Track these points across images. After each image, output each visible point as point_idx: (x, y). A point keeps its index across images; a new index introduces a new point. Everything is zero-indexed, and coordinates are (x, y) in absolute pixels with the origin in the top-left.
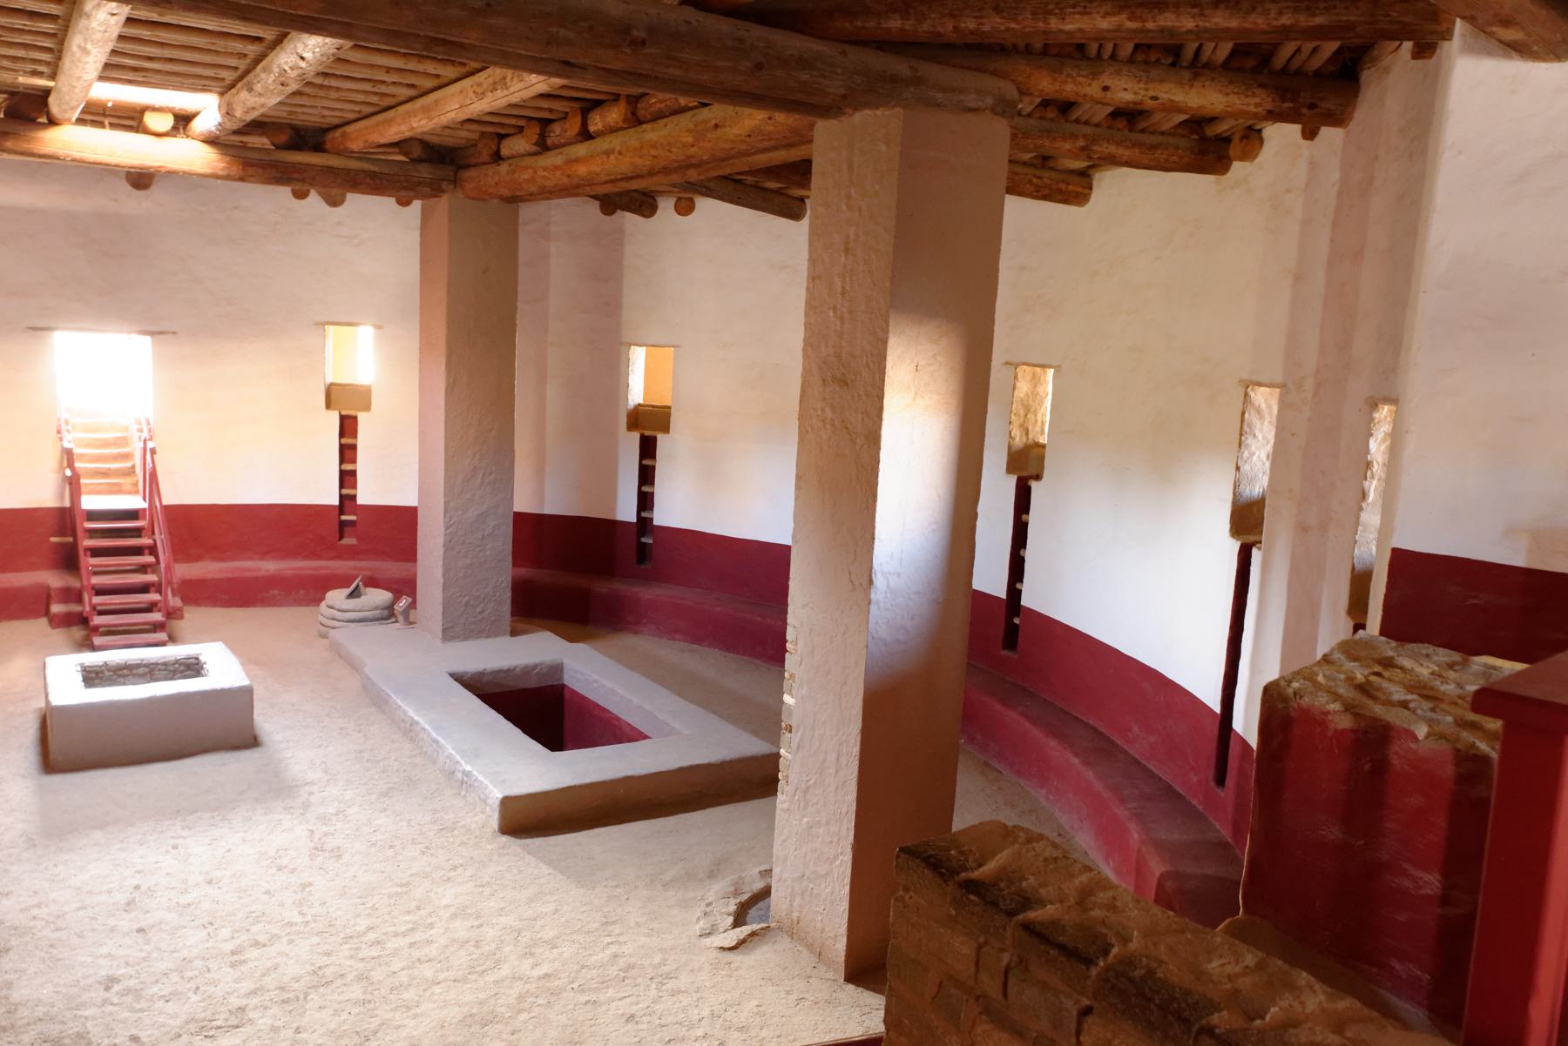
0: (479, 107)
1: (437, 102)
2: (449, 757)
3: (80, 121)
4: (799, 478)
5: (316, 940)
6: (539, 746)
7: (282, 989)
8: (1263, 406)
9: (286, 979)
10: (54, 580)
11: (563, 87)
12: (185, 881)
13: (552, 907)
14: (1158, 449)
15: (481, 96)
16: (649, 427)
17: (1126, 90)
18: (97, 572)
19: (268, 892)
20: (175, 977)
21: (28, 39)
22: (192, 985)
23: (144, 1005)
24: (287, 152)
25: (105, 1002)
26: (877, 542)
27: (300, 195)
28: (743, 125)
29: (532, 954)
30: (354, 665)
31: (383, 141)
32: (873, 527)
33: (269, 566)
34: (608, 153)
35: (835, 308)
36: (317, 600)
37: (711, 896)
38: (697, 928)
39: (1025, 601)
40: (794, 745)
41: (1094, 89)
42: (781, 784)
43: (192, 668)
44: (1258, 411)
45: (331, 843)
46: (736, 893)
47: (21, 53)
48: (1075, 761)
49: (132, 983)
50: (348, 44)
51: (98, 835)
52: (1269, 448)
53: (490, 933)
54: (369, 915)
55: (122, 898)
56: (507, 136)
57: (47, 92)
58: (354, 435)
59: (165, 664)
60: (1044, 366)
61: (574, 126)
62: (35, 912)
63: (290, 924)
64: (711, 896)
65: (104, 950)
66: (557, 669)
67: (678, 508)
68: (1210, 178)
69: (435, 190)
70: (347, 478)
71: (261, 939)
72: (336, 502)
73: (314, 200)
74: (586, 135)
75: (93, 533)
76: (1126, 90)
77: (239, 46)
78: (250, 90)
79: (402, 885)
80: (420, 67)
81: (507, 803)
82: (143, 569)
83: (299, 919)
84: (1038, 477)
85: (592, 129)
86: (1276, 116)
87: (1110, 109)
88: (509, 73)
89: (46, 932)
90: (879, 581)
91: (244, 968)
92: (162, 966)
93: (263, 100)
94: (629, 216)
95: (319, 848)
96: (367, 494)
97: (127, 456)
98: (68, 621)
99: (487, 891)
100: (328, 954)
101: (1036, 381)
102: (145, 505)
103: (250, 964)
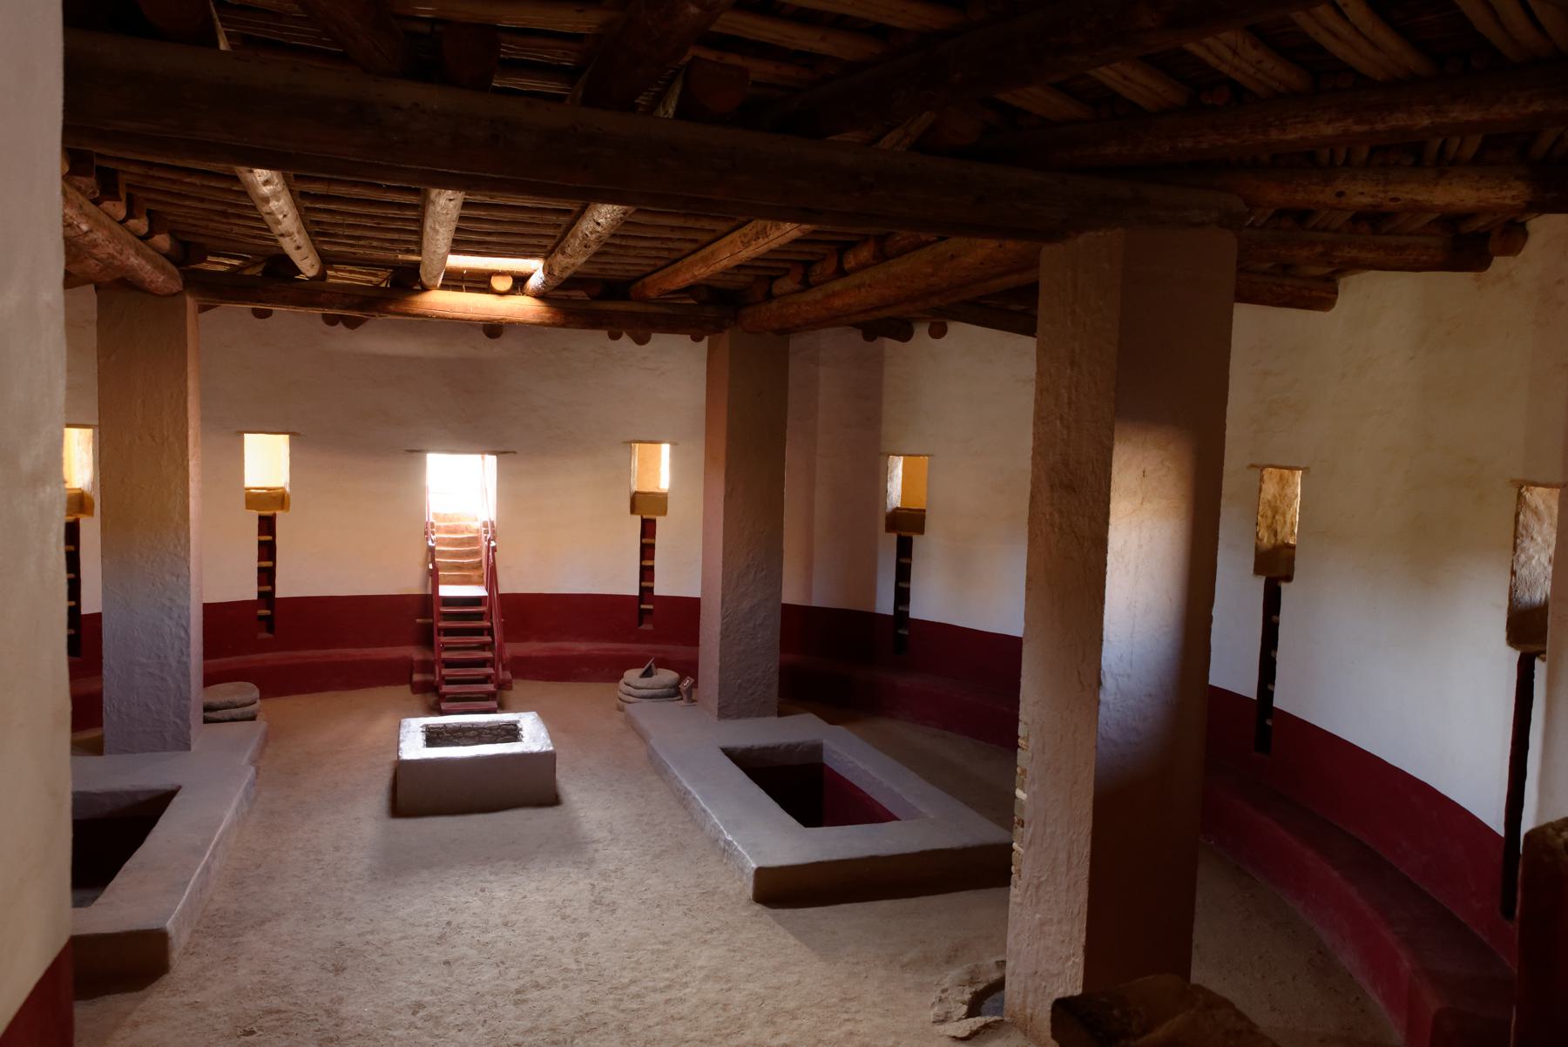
0: (746, 254)
1: (713, 253)
2: (714, 826)
3: (444, 287)
4: (1029, 579)
5: (586, 987)
6: (794, 821)
7: (553, 1030)
8: (1542, 507)
9: (558, 1021)
10: (416, 654)
11: (814, 232)
12: (487, 922)
13: (795, 978)
14: (1426, 547)
15: (746, 245)
16: (907, 525)
17: (1362, 193)
18: (449, 648)
19: (551, 938)
20: (468, 1009)
21: (399, 225)
22: (481, 1017)
23: (440, 1032)
24: (593, 302)
25: (412, 1025)
26: (1105, 643)
27: (615, 336)
28: (977, 252)
29: (774, 1023)
30: (643, 737)
31: (673, 288)
32: (1101, 630)
33: (582, 647)
34: (859, 287)
35: (1061, 418)
36: (617, 678)
37: (946, 983)
38: (931, 1014)
39: (1278, 702)
40: (1027, 837)
41: (1327, 196)
42: (1014, 877)
43: (511, 733)
44: (1536, 512)
45: (609, 897)
46: (972, 982)
47: (396, 236)
48: (1335, 874)
49: (434, 1010)
50: (631, 209)
51: (425, 874)
52: (1551, 551)
53: (737, 997)
54: (633, 969)
55: (435, 931)
56: (777, 277)
57: (417, 265)
58: (653, 535)
59: (491, 729)
60: (1292, 469)
61: (830, 266)
62: (369, 937)
63: (567, 970)
64: (946, 983)
65: (416, 978)
66: (817, 749)
67: (935, 600)
68: (1471, 275)
69: (718, 328)
70: (647, 573)
71: (542, 981)
72: (636, 593)
73: (625, 341)
74: (841, 272)
75: (448, 616)
76: (1362, 193)
77: (553, 218)
78: (563, 253)
79: (664, 943)
80: (698, 225)
81: (761, 873)
82: (483, 647)
83: (574, 966)
84: (1289, 578)
85: (847, 266)
86: (1541, 207)
87: (1349, 215)
88: (769, 224)
89: (375, 957)
90: (1108, 682)
91: (525, 1007)
92: (460, 997)
93: (572, 261)
94: (887, 340)
95: (597, 902)
96: (661, 588)
97: (476, 553)
98: (420, 689)
99: (738, 956)
100: (595, 1002)
101: (1283, 483)
102: (485, 593)
103: (531, 1004)
